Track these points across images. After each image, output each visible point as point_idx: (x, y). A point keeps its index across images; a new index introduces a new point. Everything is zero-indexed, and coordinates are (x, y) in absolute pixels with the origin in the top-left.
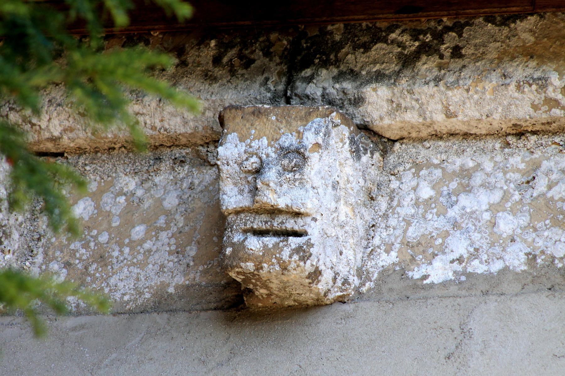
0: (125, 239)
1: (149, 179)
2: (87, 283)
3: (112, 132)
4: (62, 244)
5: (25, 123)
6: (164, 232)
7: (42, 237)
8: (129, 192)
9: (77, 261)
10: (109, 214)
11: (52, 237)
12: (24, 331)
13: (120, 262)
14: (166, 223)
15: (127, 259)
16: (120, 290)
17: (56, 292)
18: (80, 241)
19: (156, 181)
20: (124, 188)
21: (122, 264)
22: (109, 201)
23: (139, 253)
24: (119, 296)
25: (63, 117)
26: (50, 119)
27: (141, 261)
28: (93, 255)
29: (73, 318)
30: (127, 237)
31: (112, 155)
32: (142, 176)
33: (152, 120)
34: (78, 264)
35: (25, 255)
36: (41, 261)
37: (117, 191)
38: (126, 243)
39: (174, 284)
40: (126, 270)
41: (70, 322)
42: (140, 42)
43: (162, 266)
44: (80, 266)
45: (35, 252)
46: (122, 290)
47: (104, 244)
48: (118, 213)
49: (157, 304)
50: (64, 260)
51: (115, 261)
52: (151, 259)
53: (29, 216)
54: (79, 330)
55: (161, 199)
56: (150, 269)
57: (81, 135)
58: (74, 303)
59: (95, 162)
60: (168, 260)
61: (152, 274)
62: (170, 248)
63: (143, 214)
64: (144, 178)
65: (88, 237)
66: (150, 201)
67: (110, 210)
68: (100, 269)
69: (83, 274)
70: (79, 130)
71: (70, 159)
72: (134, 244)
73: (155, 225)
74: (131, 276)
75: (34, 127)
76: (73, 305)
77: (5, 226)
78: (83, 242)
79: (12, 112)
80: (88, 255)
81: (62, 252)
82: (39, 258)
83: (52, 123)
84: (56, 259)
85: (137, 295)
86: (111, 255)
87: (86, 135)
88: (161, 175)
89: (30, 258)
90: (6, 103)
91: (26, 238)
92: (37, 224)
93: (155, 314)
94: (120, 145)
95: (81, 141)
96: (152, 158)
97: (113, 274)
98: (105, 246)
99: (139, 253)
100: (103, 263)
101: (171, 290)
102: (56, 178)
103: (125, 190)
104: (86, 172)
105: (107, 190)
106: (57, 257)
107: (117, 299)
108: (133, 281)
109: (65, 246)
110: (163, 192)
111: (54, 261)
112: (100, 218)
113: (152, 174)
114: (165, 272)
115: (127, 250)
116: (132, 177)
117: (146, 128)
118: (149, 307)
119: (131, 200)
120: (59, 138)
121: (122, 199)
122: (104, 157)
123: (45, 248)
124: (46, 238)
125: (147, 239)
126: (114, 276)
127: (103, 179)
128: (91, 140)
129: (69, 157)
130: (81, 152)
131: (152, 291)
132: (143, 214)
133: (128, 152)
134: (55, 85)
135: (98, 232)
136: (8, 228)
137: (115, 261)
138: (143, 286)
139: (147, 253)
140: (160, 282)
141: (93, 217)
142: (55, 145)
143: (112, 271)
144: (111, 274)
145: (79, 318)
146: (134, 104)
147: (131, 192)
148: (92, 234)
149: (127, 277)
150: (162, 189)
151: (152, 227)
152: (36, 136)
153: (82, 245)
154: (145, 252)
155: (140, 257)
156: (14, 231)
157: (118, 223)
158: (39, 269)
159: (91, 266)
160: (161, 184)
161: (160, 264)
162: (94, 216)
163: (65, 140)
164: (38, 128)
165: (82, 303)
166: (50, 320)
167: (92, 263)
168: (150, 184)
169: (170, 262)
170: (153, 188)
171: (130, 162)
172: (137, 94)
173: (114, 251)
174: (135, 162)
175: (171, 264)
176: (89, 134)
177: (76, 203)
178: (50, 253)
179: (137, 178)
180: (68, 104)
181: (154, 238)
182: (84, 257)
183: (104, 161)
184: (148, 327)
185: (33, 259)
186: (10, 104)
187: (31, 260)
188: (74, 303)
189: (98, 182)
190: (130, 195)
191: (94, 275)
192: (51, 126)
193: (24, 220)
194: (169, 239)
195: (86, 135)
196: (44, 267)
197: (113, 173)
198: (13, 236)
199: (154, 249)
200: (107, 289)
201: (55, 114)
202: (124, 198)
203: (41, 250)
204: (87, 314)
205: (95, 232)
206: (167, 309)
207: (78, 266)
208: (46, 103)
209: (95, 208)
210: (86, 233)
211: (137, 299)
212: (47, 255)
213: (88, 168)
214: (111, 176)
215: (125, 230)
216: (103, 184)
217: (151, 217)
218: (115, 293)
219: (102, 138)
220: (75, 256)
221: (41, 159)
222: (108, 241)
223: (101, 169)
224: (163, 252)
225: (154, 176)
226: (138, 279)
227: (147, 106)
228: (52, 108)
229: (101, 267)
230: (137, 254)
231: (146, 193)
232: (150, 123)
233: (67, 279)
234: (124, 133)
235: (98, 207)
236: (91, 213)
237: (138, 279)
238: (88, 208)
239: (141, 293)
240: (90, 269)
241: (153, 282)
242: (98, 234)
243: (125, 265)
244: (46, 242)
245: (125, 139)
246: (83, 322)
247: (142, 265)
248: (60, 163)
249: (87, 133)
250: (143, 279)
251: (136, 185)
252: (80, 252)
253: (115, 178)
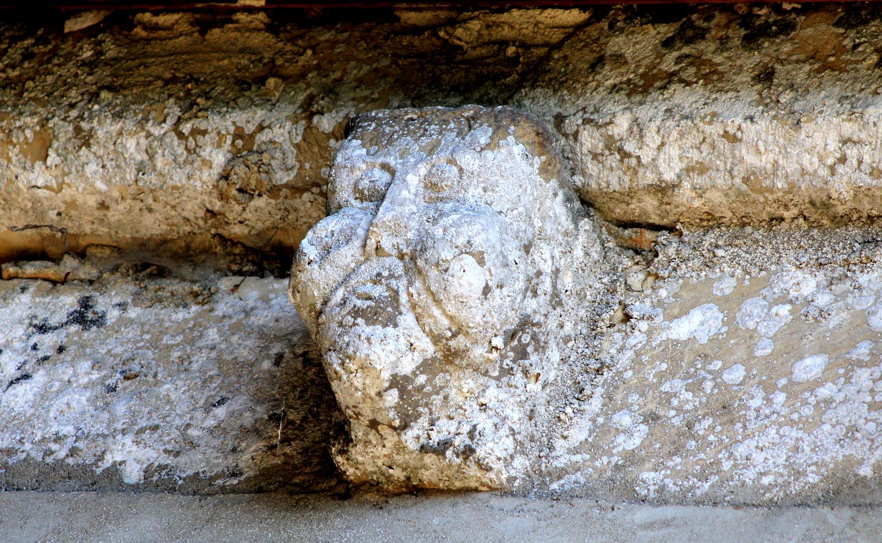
0: (778, 379)
1: (847, 276)
2: (688, 451)
3: (787, 177)
4: (645, 383)
5: (610, 150)
6: (864, 369)
7: (605, 369)
8: (800, 299)
9: (673, 413)
10: (752, 334)
11: (626, 370)
12: (542, 523)
13: (763, 417)
14: (871, 354)
15: (778, 413)
16: (755, 466)
17: (619, 463)
18: (684, 379)
19: (860, 280)
20: (791, 291)
21: (766, 422)
22: (756, 311)
23: (806, 403)
24: (752, 477)
25: (691, 140)
26: (663, 144)
27: (808, 417)
28: (708, 402)
29: (650, 508)
30: (785, 376)
31: (774, 231)
32: (833, 271)
33: (876, 155)
34: (674, 417)
35: (566, 397)
36: (597, 410)
37: (776, 296)
38: (780, 386)
39: (872, 461)
40: (774, 431)
41: (643, 514)
42: (873, 19)
43: (853, 429)
44: (676, 421)
45: (587, 392)
46: (760, 467)
47: (733, 385)
48: (771, 334)
49: (831, 495)
50: (643, 410)
51: (752, 414)
52: (830, 415)
53: (584, 331)
54: (660, 528)
55: (866, 313)
56: (826, 433)
57: (720, 182)
58: (654, 484)
59: (737, 242)
60: (866, 419)
61: (828, 442)
62: (873, 398)
63: (825, 337)
64: (836, 275)
65: (703, 372)
66: (844, 315)
67: (756, 328)
68: (719, 428)
69: (680, 434)
70: (718, 170)
71: (686, 236)
72: (797, 388)
73: (848, 356)
74: (783, 442)
75: (626, 160)
76: (652, 488)
77: (538, 324)
78: (690, 381)
79: (588, 126)
80: (697, 404)
81: (643, 395)
82: (595, 405)
83: (665, 154)
84: (628, 407)
85: (789, 477)
86: (745, 405)
87: (729, 182)
88: (873, 271)
89: (574, 401)
90: (578, 112)
91: (573, 367)
92: (601, 344)
93: (826, 509)
94: (795, 211)
95: (718, 194)
96: (859, 239)
97: (745, 438)
98: (735, 388)
99: (806, 403)
100: (725, 419)
101: (866, 471)
102: (652, 268)
103: (793, 294)
104: (715, 260)
105: (756, 293)
106: (632, 404)
107: (748, 480)
108: (785, 451)
109: (651, 386)
110: (872, 301)
111: (625, 411)
112: (732, 342)
113: (854, 268)
114: (856, 439)
115: (780, 398)
116: (812, 272)
117: (861, 171)
118: (813, 498)
119: (802, 312)
120: (674, 186)
121: (784, 310)
122: (757, 235)
123: (608, 388)
124: (614, 370)
125: (826, 381)
126: (747, 442)
127: (749, 274)
128: (740, 193)
129: (685, 232)
130: (711, 223)
131: (823, 470)
132: (825, 337)
133: (810, 227)
134: (683, 85)
135: (724, 365)
136: (543, 333)
137: (752, 414)
138: (805, 461)
139: (822, 405)
140: (844, 456)
141: (717, 339)
142: (662, 203)
143: (744, 432)
144: (740, 437)
145: (660, 509)
146: (843, 120)
147: (806, 298)
148: (712, 367)
149: (773, 443)
150: (871, 295)
151: (840, 361)
152: (627, 179)
153: (686, 385)
154: (818, 403)
155: (807, 411)
156: (552, 344)
157: (769, 351)
158: (590, 423)
159: (699, 422)
160: (872, 286)
161: (847, 424)
162: (721, 337)
163: (685, 194)
164: (634, 161)
165: (671, 485)
166: (601, 508)
167: (704, 417)
168: (847, 285)
169: (871, 423)
170: (852, 293)
171: (811, 246)
172: (852, 104)
173: (752, 397)
174: (822, 246)
175: (872, 426)
176: (738, 181)
177: (687, 313)
178: (618, 397)
179: (821, 276)
180: (706, 116)
181: (842, 380)
182: (689, 407)
183: (756, 241)
184: (808, 530)
185: (580, 406)
186: (585, 112)
187: (576, 406)
188: (654, 484)
189: (738, 279)
190: (801, 304)
191: (704, 437)
192: (661, 160)
193: (573, 335)
194: (874, 382)
195: (729, 182)
196: (601, 420)
197: (772, 264)
198: (548, 352)
199: (840, 397)
200: (727, 463)
201: (675, 134)
202: (788, 307)
203: (599, 391)
204: (680, 504)
205: (717, 365)
206: (853, 502)
207: (674, 421)
208: (661, 113)
209: (724, 323)
210: (699, 366)
211: (789, 483)
212: (611, 399)
213: (720, 253)
214: (766, 269)
215: (782, 364)
216: (747, 283)
217: (841, 342)
218: (745, 471)
219: (761, 191)
220: (670, 403)
221: (626, 232)
222: (744, 380)
223: (748, 255)
224: (857, 404)
225: (858, 272)
226: (796, 449)
227: (872, 124)
228: (670, 123)
229: (720, 425)
230: (802, 405)
231: (836, 301)
232: (869, 161)
233: (647, 443)
234: (811, 181)
235: (730, 321)
236: (714, 331)
237: (796, 449)
238: (711, 322)
239: (799, 472)
240: (697, 426)
241: (830, 455)
242: (723, 368)
243: (774, 423)
244: (613, 378)
245: (810, 197)
246: (669, 516)
247: (809, 425)
248: (665, 242)
249: (732, 178)
250: (807, 449)
251: (817, 286)
252: (681, 397)
253: (775, 273)
